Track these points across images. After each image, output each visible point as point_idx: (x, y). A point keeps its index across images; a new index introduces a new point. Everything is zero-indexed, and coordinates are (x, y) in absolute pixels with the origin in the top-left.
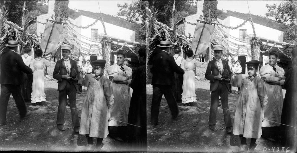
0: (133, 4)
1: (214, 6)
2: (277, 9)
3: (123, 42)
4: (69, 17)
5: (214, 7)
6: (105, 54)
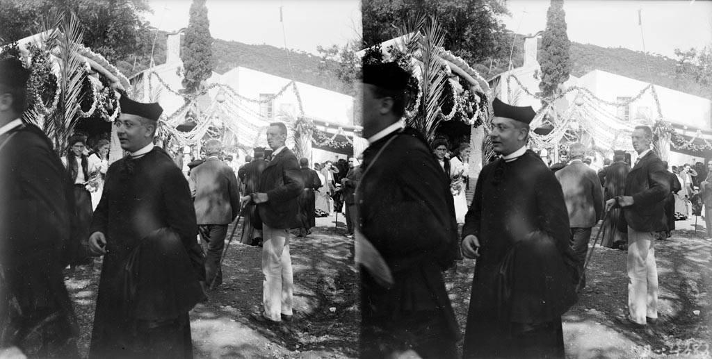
0: (350, 46)
1: (565, 51)
2: (341, 54)
3: (336, 127)
4: (570, 75)
5: (564, 53)
6: (302, 150)
